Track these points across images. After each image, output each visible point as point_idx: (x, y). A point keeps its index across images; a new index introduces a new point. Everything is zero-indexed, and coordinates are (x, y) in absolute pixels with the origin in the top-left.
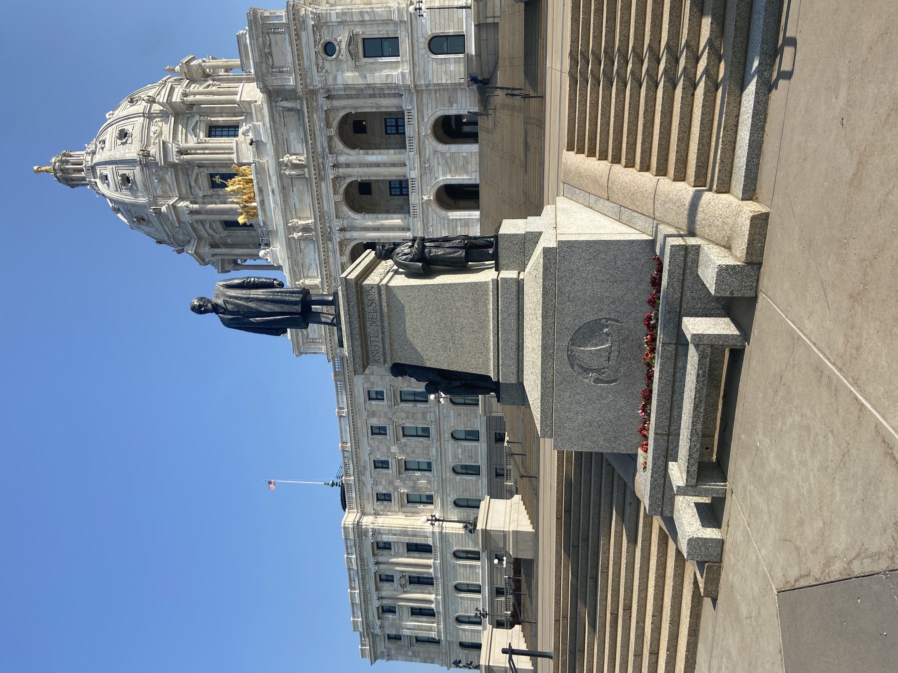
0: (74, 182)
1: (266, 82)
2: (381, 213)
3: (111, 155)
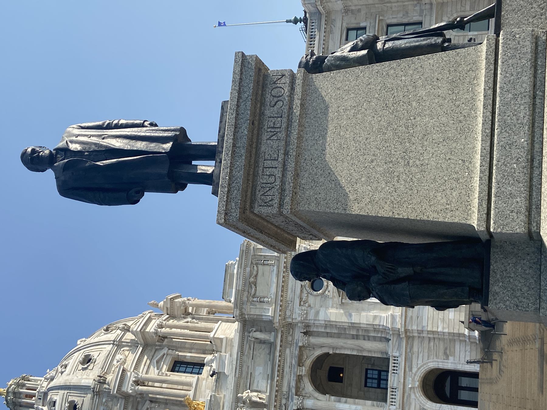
1: (243, 310)
3: (68, 380)
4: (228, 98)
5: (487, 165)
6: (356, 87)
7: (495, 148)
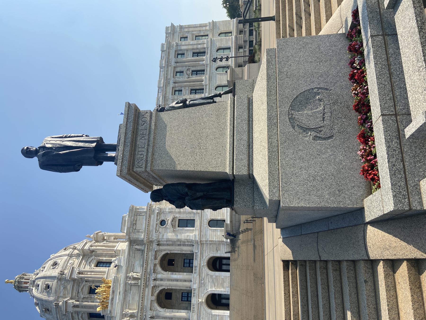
0: (22, 289)
1: (130, 236)
2: (175, 309)
3: (45, 274)
4: (122, 123)
5: (232, 148)
6: (178, 118)
7: (235, 141)
